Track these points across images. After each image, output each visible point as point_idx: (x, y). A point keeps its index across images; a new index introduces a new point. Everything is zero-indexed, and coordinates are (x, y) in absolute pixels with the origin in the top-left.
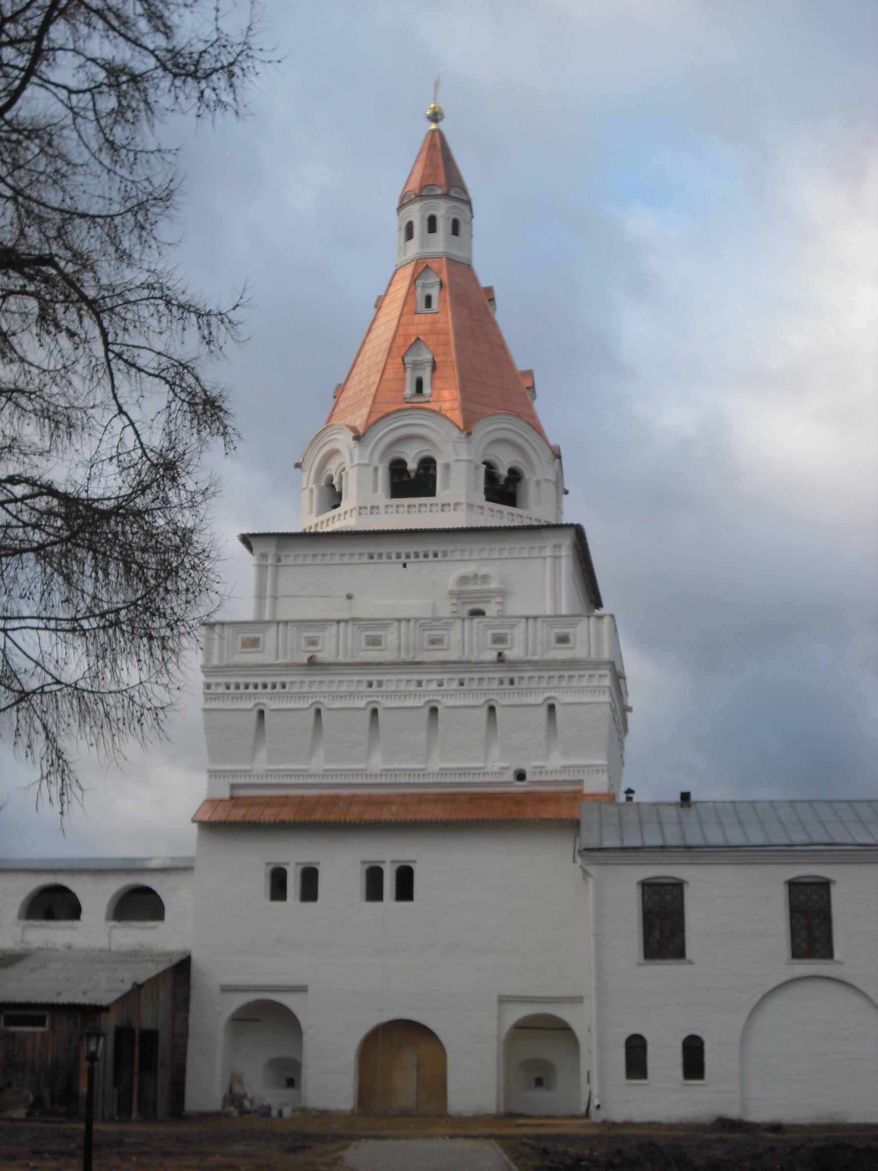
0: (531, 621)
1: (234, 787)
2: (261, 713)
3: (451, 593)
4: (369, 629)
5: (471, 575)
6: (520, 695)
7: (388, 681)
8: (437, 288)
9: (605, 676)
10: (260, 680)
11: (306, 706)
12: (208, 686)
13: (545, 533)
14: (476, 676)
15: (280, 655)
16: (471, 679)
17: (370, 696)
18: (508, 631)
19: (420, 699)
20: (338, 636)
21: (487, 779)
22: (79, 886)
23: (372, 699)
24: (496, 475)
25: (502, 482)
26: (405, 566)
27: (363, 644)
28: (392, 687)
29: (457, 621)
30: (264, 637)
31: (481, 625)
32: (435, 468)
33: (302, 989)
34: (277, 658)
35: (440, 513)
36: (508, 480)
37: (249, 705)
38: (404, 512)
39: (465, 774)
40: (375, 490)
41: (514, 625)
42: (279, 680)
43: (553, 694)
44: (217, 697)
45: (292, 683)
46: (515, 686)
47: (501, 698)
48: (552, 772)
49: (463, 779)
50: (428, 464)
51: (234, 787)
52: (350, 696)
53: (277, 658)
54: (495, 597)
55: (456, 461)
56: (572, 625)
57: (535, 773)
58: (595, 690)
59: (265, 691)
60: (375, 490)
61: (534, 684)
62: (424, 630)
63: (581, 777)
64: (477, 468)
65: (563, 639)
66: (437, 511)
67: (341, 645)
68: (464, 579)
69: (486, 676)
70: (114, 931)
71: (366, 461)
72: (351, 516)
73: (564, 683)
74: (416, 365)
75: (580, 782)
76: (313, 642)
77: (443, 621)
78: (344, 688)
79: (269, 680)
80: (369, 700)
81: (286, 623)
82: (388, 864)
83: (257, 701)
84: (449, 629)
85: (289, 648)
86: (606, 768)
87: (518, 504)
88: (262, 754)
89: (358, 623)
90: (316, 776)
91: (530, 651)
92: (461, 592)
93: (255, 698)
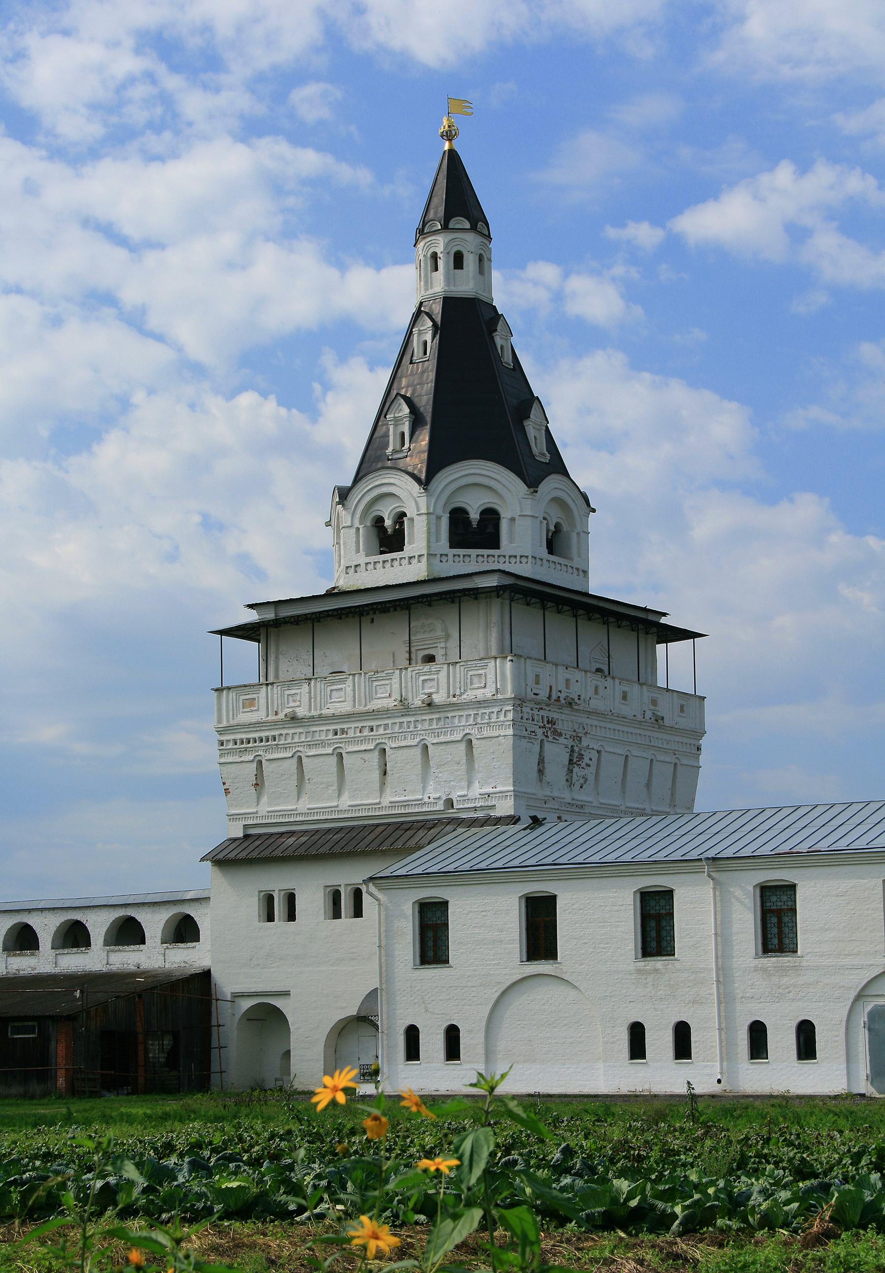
12: (222, 743)
18: (435, 676)
20: (310, 693)
22: (143, 917)
30: (258, 697)
33: (286, 994)
34: (310, 710)
40: (358, 551)
44: (230, 752)
52: (322, 743)
53: (310, 710)
64: (439, 518)
69: (420, 718)
70: (167, 951)
72: (419, 561)
79: (263, 734)
82: (342, 886)
86: (512, 793)
88: (264, 799)
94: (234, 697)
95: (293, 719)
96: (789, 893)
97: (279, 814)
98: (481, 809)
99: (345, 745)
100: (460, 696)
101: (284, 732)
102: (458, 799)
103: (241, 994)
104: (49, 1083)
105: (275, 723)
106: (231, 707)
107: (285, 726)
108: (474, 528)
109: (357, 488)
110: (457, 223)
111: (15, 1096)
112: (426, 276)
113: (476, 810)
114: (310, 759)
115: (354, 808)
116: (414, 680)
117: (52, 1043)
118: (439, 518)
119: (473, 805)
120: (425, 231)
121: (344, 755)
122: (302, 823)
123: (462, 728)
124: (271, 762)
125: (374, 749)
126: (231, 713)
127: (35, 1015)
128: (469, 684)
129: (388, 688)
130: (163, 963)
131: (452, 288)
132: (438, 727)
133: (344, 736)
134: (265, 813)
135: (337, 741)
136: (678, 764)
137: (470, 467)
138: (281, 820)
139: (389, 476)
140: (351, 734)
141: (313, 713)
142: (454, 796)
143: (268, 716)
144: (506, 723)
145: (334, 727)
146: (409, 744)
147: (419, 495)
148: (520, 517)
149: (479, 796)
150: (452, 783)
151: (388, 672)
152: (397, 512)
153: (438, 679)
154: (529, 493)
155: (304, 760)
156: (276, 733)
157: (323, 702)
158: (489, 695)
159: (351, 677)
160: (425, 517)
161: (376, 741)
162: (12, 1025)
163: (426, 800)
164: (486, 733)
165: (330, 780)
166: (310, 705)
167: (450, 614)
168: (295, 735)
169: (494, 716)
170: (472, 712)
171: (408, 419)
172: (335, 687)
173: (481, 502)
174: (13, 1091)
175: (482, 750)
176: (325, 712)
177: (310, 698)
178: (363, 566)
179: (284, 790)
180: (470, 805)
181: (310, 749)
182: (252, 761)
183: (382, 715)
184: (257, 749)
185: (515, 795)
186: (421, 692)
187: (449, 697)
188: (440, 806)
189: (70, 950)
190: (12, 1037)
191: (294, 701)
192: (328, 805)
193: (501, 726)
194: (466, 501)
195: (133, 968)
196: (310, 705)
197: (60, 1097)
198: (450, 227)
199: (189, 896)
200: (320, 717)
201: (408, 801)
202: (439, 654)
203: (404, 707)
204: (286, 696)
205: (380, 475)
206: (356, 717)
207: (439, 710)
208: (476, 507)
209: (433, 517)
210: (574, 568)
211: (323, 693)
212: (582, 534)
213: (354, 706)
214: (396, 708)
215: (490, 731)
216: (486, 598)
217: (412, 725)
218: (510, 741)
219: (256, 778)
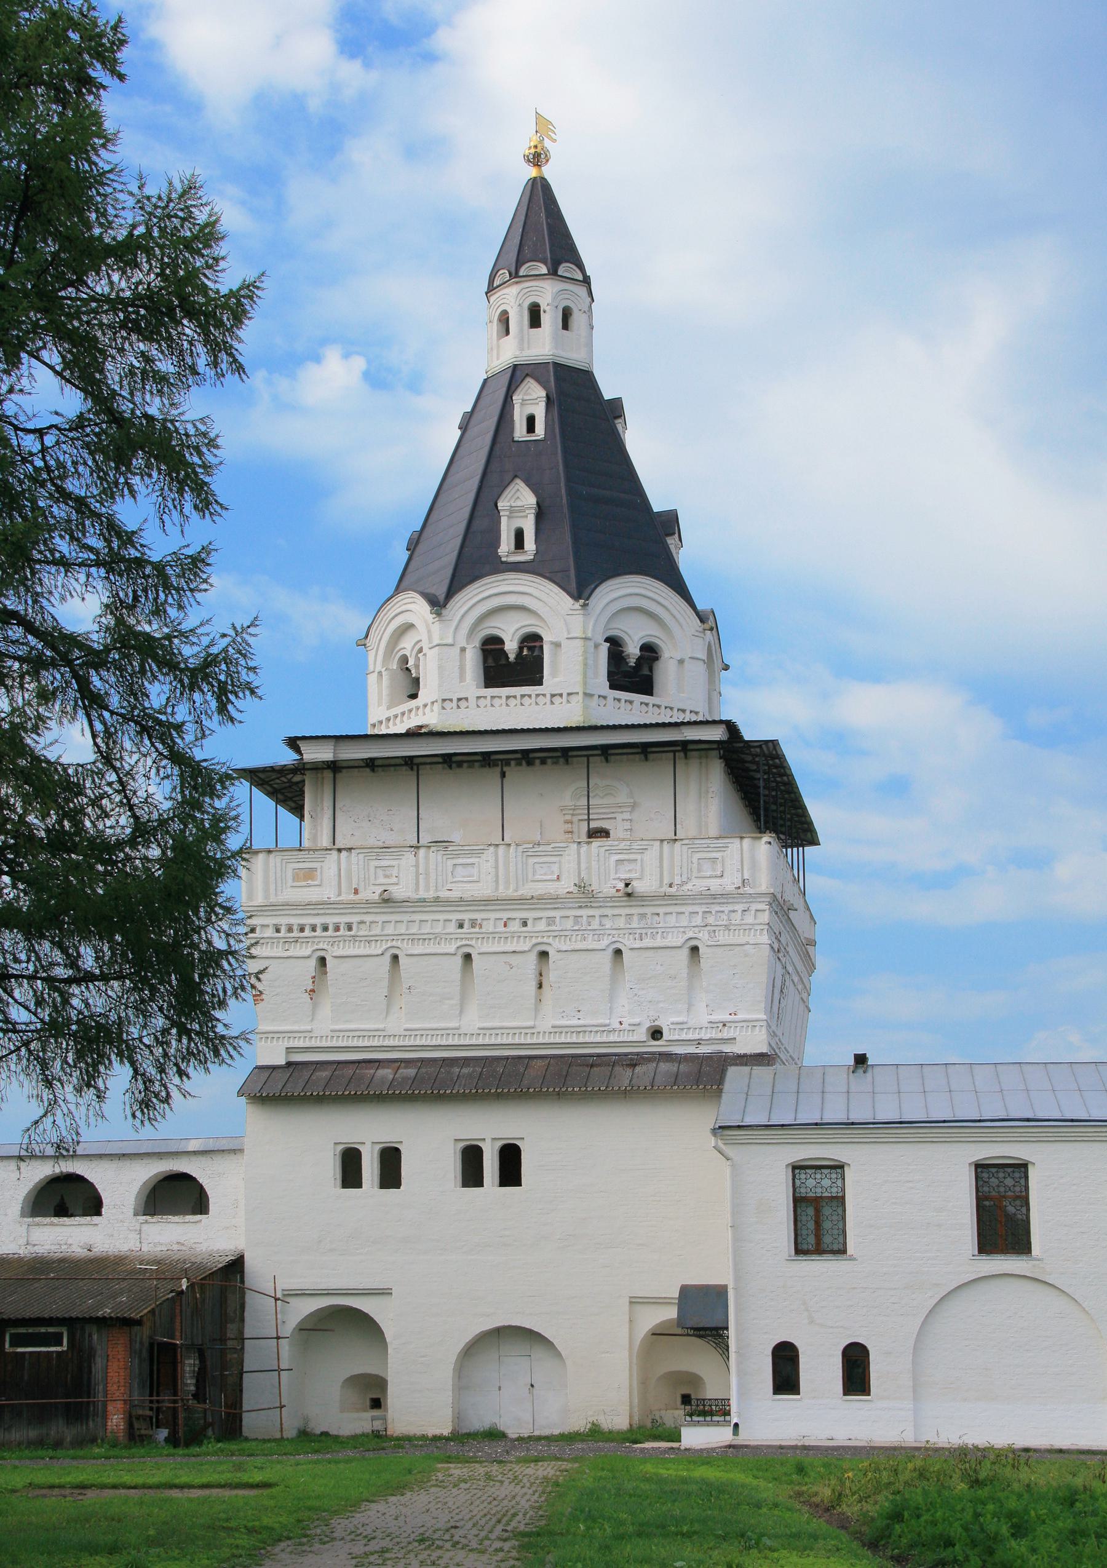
18: (638, 857)
20: (417, 866)
33: (385, 1292)
40: (462, 678)
50: (532, 641)
52: (436, 938)
60: (462, 678)
70: (145, 1227)
71: (450, 641)
78: (426, 929)
80: (459, 943)
86: (764, 1023)
94: (279, 864)
95: (387, 901)
96: (1017, 1175)
97: (351, 1034)
98: (710, 1042)
99: (476, 943)
100: (684, 883)
101: (368, 918)
102: (672, 1027)
103: (300, 1292)
104: (91, 1423)
105: (353, 905)
106: (272, 879)
107: (369, 910)
108: (631, 667)
109: (465, 593)
110: (566, 271)
111: (19, 1444)
113: (699, 1044)
114: (635, 953)
115: (488, 1032)
116: (602, 859)
117: (98, 1360)
118: (596, 646)
119: (697, 1037)
122: (393, 1048)
123: (682, 930)
124: (343, 960)
126: (272, 887)
127: (66, 1316)
128: (695, 870)
129: (555, 868)
130: (138, 1245)
131: (527, 353)
132: (642, 926)
133: (477, 930)
135: (463, 936)
138: (355, 1043)
139: (517, 582)
140: (488, 927)
141: (422, 894)
142: (664, 1024)
143: (339, 895)
144: (757, 927)
145: (460, 916)
146: (590, 947)
147: (571, 612)
148: (691, 660)
150: (661, 1005)
151: (557, 845)
153: (642, 860)
154: (701, 629)
156: (354, 919)
157: (440, 881)
158: (730, 888)
159: (492, 848)
161: (386, 944)
162: (13, 1331)
163: (617, 1026)
164: (723, 937)
166: (417, 884)
167: (659, 772)
168: (373, 925)
169: (739, 915)
170: (700, 909)
172: (460, 861)
173: (644, 633)
174: (15, 1435)
176: (444, 894)
177: (417, 874)
178: (472, 701)
179: (362, 1001)
180: (690, 1036)
181: (413, 944)
183: (546, 903)
184: (316, 940)
186: (613, 876)
187: (661, 886)
189: (48, 1220)
190: (11, 1350)
191: (386, 876)
192: (442, 1025)
193: (751, 927)
194: (626, 629)
195: (79, 1250)
196: (417, 884)
197: (114, 1445)
199: (192, 1146)
200: (437, 900)
201: (585, 1026)
202: (617, 829)
203: (585, 895)
204: (372, 870)
205: (504, 580)
206: (500, 905)
207: (643, 903)
208: (636, 638)
209: (591, 644)
211: (440, 868)
213: (497, 889)
214: (568, 896)
216: (700, 757)
217: (596, 921)
219: (313, 982)
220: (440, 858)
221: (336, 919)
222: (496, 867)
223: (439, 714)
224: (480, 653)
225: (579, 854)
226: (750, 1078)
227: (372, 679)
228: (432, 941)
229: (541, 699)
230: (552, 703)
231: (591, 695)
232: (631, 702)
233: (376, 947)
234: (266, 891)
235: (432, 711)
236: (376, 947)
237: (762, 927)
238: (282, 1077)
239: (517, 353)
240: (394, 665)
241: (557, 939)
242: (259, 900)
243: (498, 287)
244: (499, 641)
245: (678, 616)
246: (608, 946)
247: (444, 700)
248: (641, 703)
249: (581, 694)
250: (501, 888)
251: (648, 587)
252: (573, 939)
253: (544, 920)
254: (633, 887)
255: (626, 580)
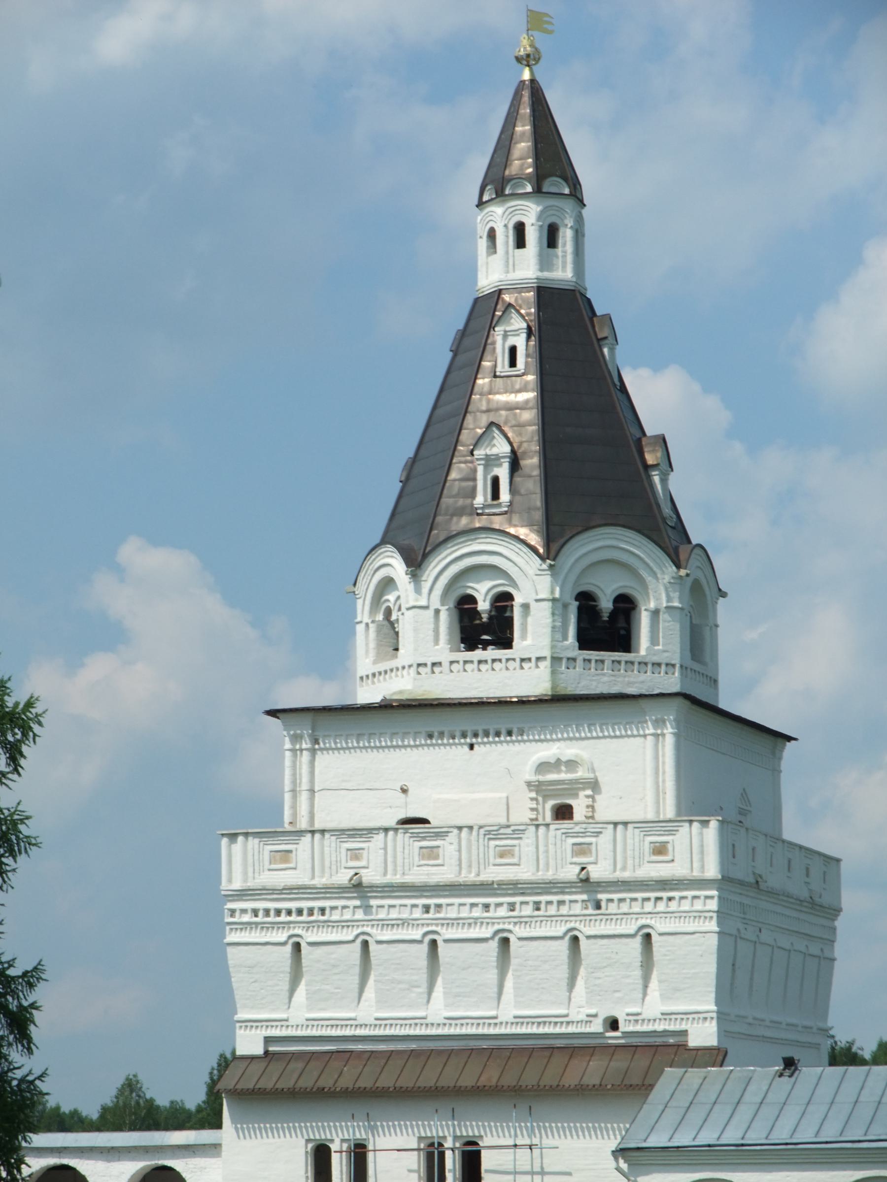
0: (620, 828)
1: (268, 1040)
2: (297, 947)
3: (529, 784)
4: (424, 838)
5: (553, 761)
6: (608, 922)
7: (448, 905)
8: (524, 336)
9: (712, 897)
10: (293, 905)
11: (351, 938)
13: (643, 703)
14: (555, 898)
15: (317, 873)
16: (549, 903)
17: (428, 925)
18: (593, 840)
19: (487, 928)
21: (571, 1029)
23: (430, 928)
24: (597, 608)
25: (605, 617)
26: (471, 747)
27: (416, 858)
28: (452, 913)
29: (530, 827)
30: (296, 849)
31: (559, 832)
32: (512, 611)
34: (313, 877)
35: (519, 672)
36: (614, 614)
37: (282, 936)
38: (473, 671)
39: (545, 1023)
40: (436, 641)
41: (600, 833)
42: (317, 904)
43: (648, 922)
45: (333, 908)
46: (603, 911)
47: (585, 926)
48: (649, 1020)
49: (541, 1030)
50: (503, 600)
51: (268, 1040)
52: (403, 924)
53: (385, 874)
54: (584, 789)
55: (537, 601)
56: (671, 832)
57: (630, 1021)
58: (699, 915)
59: (300, 919)
60: (436, 641)
61: (625, 908)
62: (490, 839)
63: (683, 1027)
64: (565, 606)
65: (660, 850)
66: (515, 669)
67: (390, 859)
68: (543, 767)
69: (567, 898)
71: (423, 602)
73: (661, 906)
74: (491, 461)
75: (684, 1033)
76: (355, 854)
77: (513, 828)
78: (394, 914)
79: (305, 905)
80: (426, 929)
81: (323, 832)
83: (291, 932)
84: (520, 838)
85: (327, 864)
86: (714, 1015)
87: (632, 649)
89: (410, 831)
90: (366, 1025)
91: (619, 866)
92: (540, 783)
93: (289, 928)
94: (256, 846)
110: (552, 185)
112: (507, 253)
115: (453, 1022)
116: (559, 842)
118: (565, 606)
120: (507, 192)
121: (440, 943)
125: (492, 938)
126: (250, 870)
131: (546, 274)
134: (301, 1021)
136: (758, 942)
137: (605, 536)
149: (660, 1016)
152: (499, 592)
155: (373, 947)
157: (406, 864)
160: (547, 605)
165: (415, 978)
171: (508, 460)
173: (621, 584)
175: (668, 951)
178: (446, 664)
182: (284, 944)
185: (718, 1018)
188: (597, 1027)
198: (544, 190)
209: (559, 605)
210: (684, 668)
211: (406, 851)
212: (714, 628)
213: (460, 873)
215: (689, 923)
218: (714, 940)
220: (407, 839)
221: (311, 904)
222: (460, 851)
223: (415, 679)
224: (455, 613)
225: (537, 837)
226: (679, 1084)
227: (360, 628)
228: (400, 926)
229: (511, 664)
230: (522, 668)
231: (560, 659)
232: (602, 662)
233: (347, 933)
234: (245, 873)
235: (409, 674)
236: (347, 933)
237: (711, 914)
238: (256, 1068)
239: (503, 277)
240: (380, 617)
241: (518, 926)
242: (237, 885)
243: (487, 202)
244: (472, 600)
245: (652, 564)
246: (566, 934)
247: (419, 665)
248: (613, 661)
249: (549, 659)
250: (464, 872)
251: (620, 537)
252: (533, 925)
253: (505, 906)
254: (588, 873)
255: (595, 533)
